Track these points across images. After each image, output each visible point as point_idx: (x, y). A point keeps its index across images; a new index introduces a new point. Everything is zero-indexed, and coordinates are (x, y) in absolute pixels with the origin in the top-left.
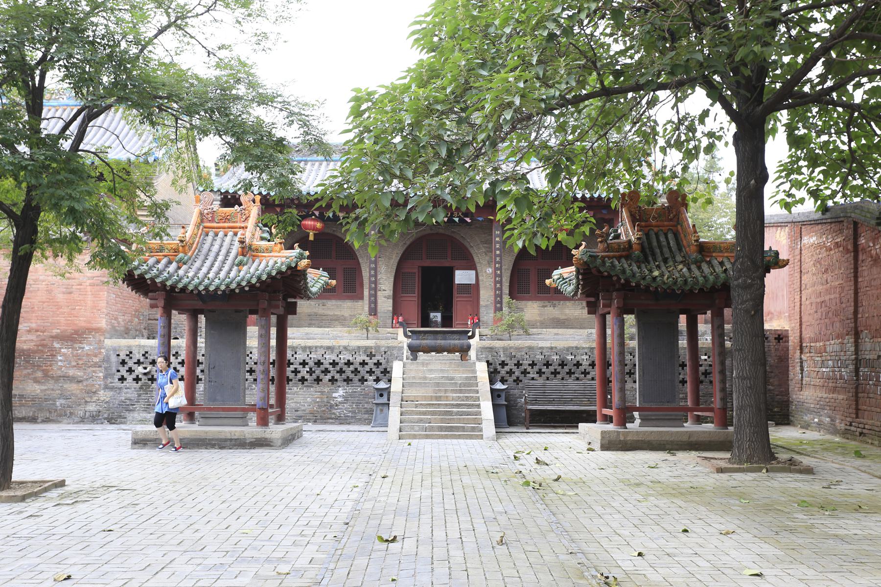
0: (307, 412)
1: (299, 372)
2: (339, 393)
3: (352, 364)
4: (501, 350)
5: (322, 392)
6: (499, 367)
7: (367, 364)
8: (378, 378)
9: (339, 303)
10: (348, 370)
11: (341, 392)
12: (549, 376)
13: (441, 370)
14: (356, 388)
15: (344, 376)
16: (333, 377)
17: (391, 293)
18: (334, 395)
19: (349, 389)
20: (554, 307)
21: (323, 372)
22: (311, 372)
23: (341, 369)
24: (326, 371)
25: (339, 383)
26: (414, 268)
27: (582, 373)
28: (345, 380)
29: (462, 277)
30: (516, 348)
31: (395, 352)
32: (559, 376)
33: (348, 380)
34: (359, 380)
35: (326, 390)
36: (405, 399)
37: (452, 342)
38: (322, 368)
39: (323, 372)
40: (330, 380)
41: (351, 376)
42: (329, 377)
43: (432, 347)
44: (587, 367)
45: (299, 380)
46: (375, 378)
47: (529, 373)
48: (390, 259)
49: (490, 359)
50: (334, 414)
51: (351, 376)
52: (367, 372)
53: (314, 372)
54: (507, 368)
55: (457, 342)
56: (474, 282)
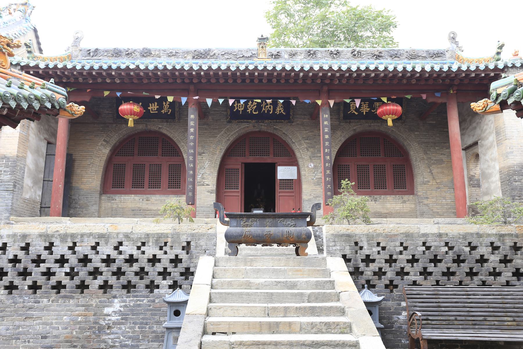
0: (62, 339)
1: (54, 274)
2: (115, 306)
3: (137, 261)
4: (364, 239)
5: (87, 307)
6: (362, 266)
7: (159, 261)
8: (175, 282)
9: (163, 197)
10: (130, 271)
11: (117, 305)
12: (440, 278)
13: (275, 271)
14: (142, 299)
15: (123, 280)
16: (106, 282)
17: (214, 188)
18: (107, 310)
19: (130, 301)
20: (375, 201)
21: (90, 274)
22: (71, 274)
23: (119, 269)
24: (95, 273)
25: (114, 292)
26: (237, 164)
27: (490, 274)
28: (124, 287)
29: (284, 173)
30: (387, 236)
31: (202, 242)
32: (455, 279)
33: (128, 287)
34: (147, 287)
35: (94, 302)
36: (210, 329)
37: (286, 229)
38: (90, 267)
39: (90, 274)
40: (101, 287)
41: (135, 280)
42: (100, 281)
43: (258, 236)
44: (497, 265)
45: (53, 288)
46: (171, 282)
47: (407, 274)
48: (214, 154)
49: (348, 252)
50: (104, 341)
51: (135, 280)
52: (160, 274)
53: (77, 274)
54: (374, 267)
55: (292, 229)
56: (295, 177)
